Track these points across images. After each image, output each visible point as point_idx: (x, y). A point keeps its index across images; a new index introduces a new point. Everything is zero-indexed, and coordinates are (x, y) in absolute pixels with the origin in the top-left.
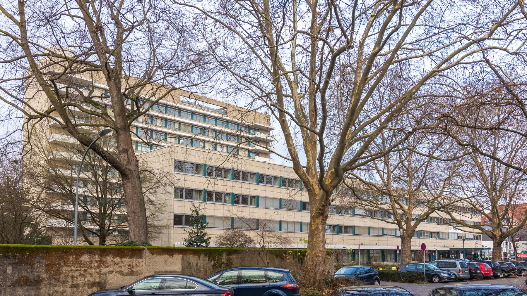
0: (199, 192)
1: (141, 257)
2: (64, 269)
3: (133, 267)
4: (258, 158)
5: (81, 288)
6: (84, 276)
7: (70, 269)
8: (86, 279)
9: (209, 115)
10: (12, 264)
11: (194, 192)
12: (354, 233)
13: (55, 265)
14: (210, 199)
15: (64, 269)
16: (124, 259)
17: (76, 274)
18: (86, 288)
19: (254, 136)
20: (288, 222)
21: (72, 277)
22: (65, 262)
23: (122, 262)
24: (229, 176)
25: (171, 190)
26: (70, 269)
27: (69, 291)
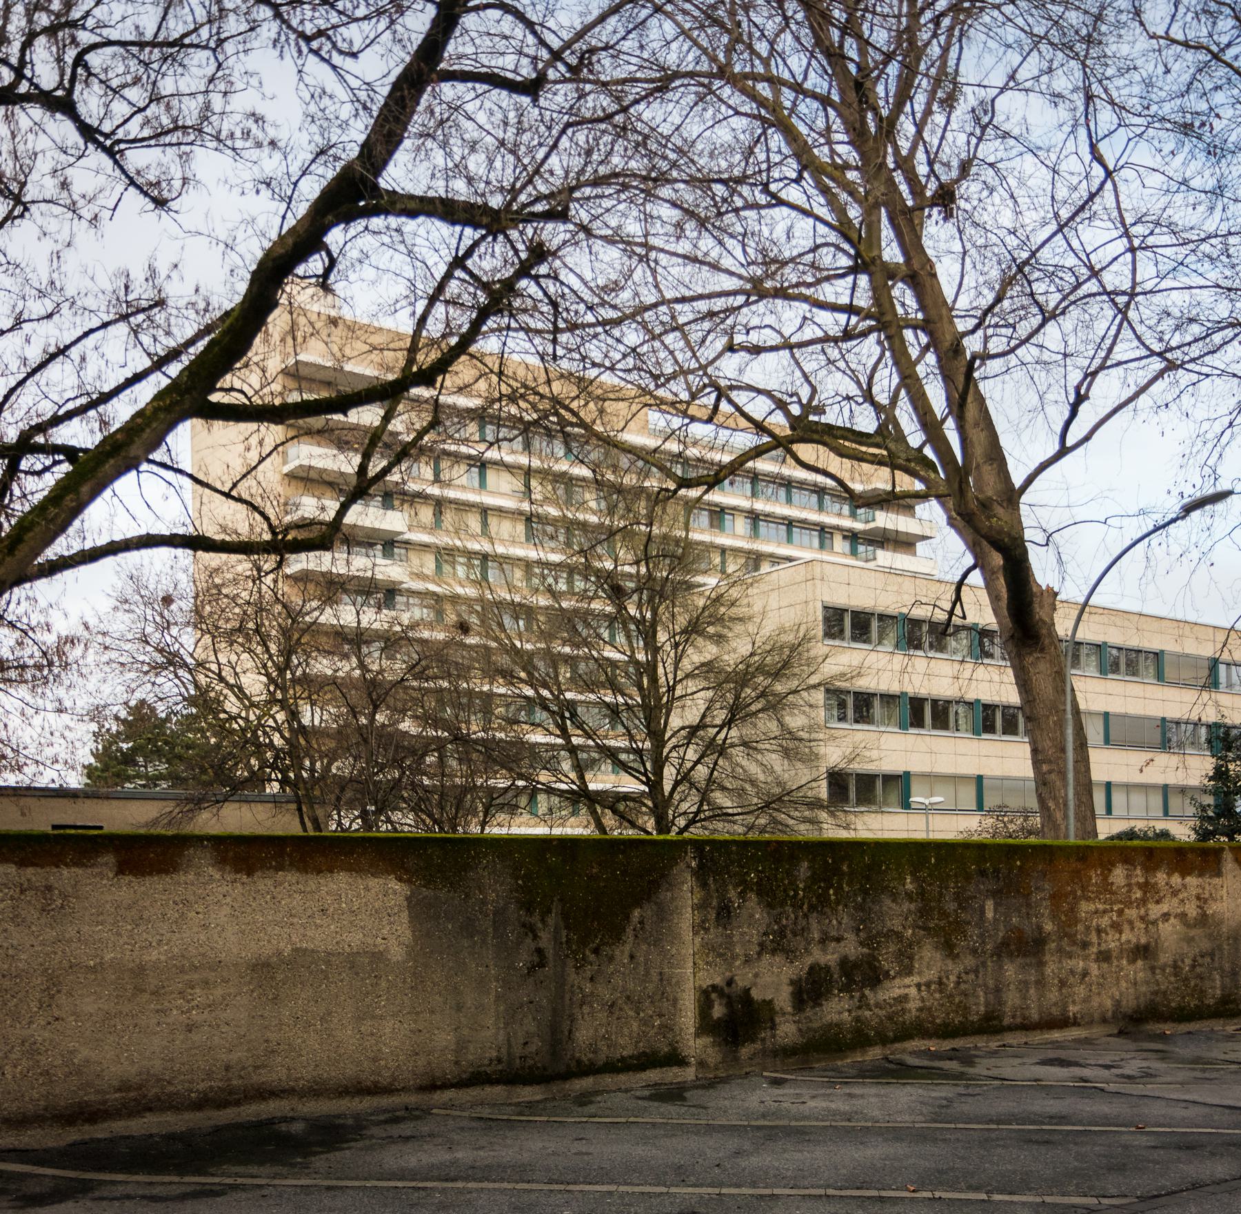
0: (889, 699)
1: (1219, 874)
2: (1085, 907)
3: (1206, 901)
4: (885, 557)
5: (1115, 963)
6: (1117, 927)
7: (1092, 907)
8: (1124, 938)
9: (804, 521)
10: (995, 894)
11: (877, 703)
12: (1160, 677)
13: (1067, 895)
14: (917, 722)
15: (1085, 907)
16: (1188, 879)
17: (1105, 922)
18: (1125, 962)
19: (872, 525)
20: (1128, 787)
21: (1099, 931)
22: (1083, 888)
23: (1185, 886)
24: (892, 636)
25: (819, 696)
26: (1092, 907)
27: (1094, 969)
